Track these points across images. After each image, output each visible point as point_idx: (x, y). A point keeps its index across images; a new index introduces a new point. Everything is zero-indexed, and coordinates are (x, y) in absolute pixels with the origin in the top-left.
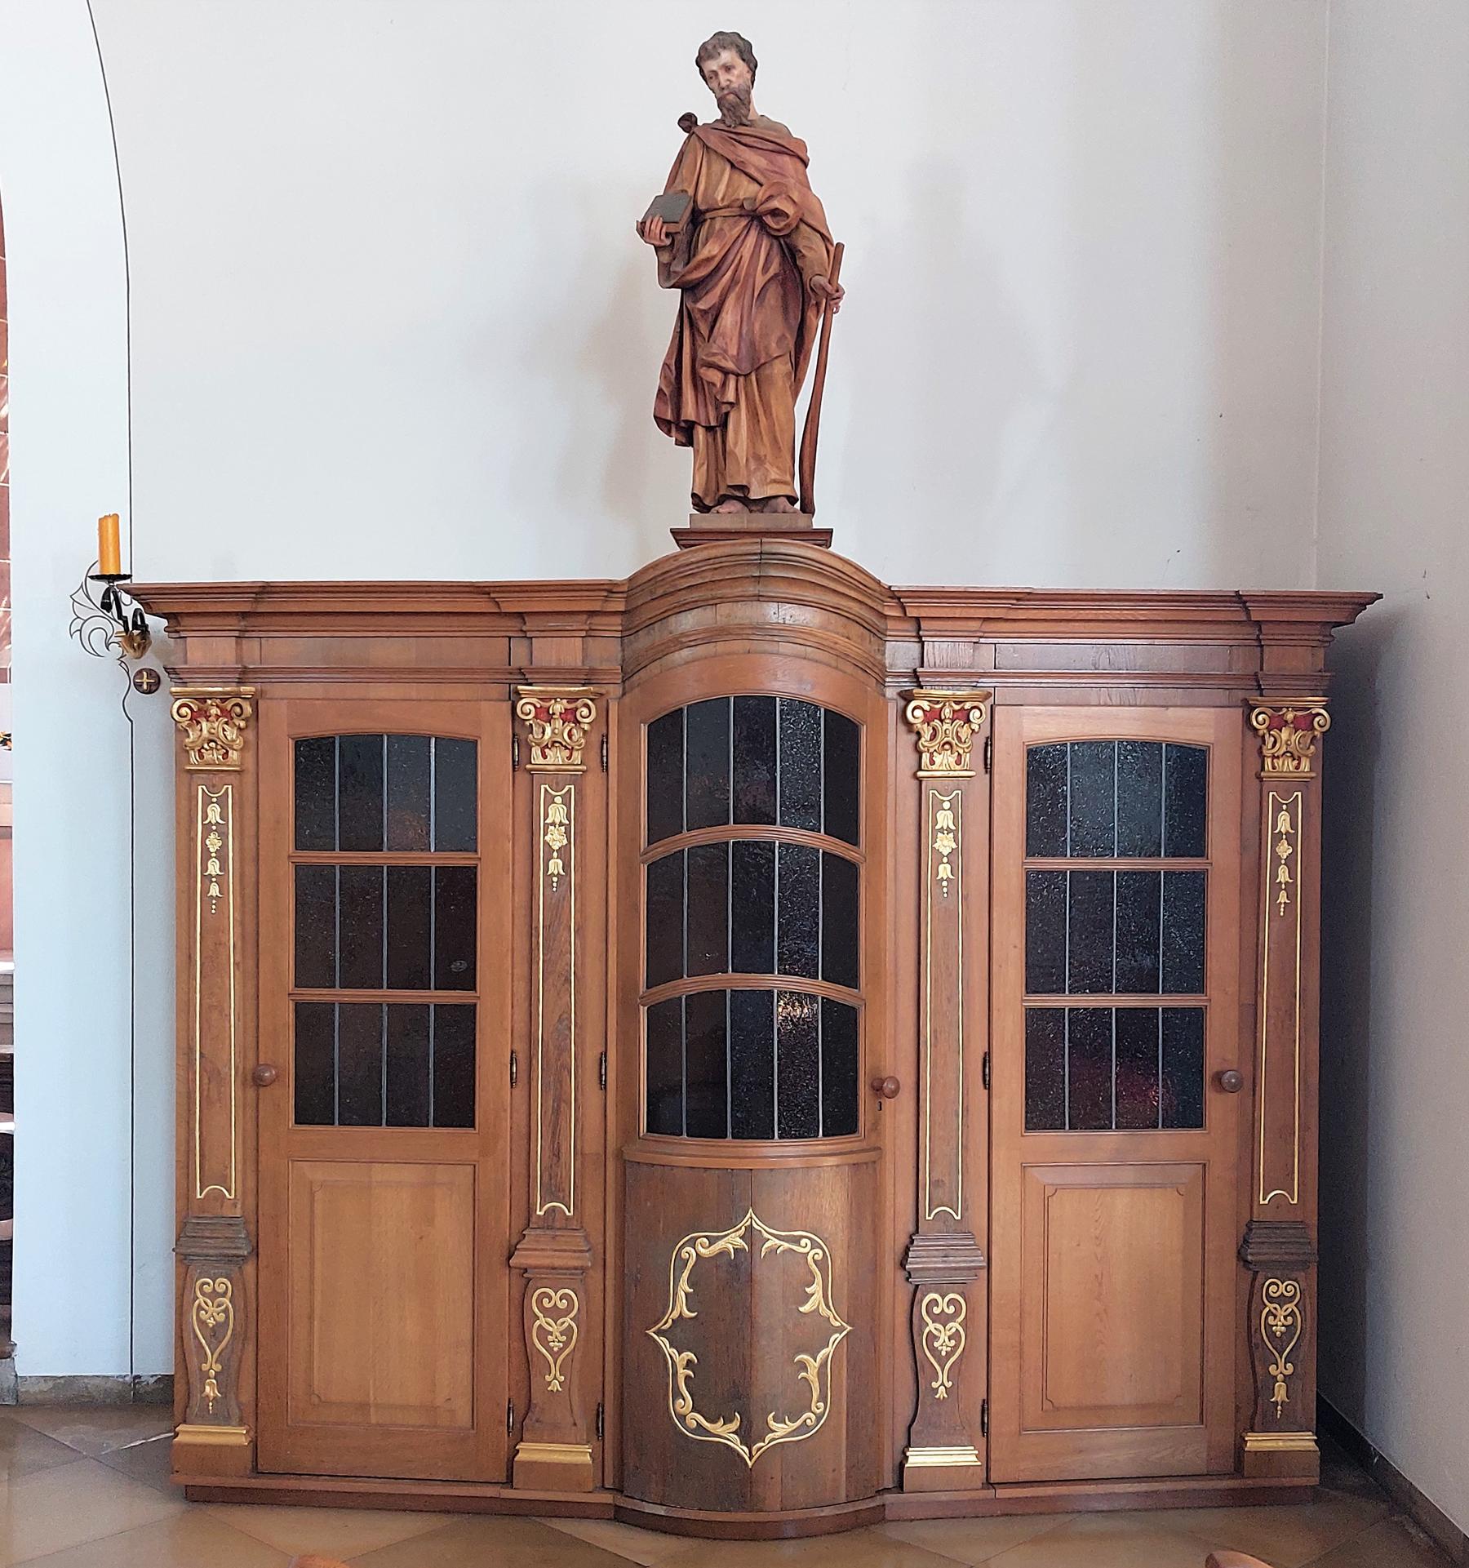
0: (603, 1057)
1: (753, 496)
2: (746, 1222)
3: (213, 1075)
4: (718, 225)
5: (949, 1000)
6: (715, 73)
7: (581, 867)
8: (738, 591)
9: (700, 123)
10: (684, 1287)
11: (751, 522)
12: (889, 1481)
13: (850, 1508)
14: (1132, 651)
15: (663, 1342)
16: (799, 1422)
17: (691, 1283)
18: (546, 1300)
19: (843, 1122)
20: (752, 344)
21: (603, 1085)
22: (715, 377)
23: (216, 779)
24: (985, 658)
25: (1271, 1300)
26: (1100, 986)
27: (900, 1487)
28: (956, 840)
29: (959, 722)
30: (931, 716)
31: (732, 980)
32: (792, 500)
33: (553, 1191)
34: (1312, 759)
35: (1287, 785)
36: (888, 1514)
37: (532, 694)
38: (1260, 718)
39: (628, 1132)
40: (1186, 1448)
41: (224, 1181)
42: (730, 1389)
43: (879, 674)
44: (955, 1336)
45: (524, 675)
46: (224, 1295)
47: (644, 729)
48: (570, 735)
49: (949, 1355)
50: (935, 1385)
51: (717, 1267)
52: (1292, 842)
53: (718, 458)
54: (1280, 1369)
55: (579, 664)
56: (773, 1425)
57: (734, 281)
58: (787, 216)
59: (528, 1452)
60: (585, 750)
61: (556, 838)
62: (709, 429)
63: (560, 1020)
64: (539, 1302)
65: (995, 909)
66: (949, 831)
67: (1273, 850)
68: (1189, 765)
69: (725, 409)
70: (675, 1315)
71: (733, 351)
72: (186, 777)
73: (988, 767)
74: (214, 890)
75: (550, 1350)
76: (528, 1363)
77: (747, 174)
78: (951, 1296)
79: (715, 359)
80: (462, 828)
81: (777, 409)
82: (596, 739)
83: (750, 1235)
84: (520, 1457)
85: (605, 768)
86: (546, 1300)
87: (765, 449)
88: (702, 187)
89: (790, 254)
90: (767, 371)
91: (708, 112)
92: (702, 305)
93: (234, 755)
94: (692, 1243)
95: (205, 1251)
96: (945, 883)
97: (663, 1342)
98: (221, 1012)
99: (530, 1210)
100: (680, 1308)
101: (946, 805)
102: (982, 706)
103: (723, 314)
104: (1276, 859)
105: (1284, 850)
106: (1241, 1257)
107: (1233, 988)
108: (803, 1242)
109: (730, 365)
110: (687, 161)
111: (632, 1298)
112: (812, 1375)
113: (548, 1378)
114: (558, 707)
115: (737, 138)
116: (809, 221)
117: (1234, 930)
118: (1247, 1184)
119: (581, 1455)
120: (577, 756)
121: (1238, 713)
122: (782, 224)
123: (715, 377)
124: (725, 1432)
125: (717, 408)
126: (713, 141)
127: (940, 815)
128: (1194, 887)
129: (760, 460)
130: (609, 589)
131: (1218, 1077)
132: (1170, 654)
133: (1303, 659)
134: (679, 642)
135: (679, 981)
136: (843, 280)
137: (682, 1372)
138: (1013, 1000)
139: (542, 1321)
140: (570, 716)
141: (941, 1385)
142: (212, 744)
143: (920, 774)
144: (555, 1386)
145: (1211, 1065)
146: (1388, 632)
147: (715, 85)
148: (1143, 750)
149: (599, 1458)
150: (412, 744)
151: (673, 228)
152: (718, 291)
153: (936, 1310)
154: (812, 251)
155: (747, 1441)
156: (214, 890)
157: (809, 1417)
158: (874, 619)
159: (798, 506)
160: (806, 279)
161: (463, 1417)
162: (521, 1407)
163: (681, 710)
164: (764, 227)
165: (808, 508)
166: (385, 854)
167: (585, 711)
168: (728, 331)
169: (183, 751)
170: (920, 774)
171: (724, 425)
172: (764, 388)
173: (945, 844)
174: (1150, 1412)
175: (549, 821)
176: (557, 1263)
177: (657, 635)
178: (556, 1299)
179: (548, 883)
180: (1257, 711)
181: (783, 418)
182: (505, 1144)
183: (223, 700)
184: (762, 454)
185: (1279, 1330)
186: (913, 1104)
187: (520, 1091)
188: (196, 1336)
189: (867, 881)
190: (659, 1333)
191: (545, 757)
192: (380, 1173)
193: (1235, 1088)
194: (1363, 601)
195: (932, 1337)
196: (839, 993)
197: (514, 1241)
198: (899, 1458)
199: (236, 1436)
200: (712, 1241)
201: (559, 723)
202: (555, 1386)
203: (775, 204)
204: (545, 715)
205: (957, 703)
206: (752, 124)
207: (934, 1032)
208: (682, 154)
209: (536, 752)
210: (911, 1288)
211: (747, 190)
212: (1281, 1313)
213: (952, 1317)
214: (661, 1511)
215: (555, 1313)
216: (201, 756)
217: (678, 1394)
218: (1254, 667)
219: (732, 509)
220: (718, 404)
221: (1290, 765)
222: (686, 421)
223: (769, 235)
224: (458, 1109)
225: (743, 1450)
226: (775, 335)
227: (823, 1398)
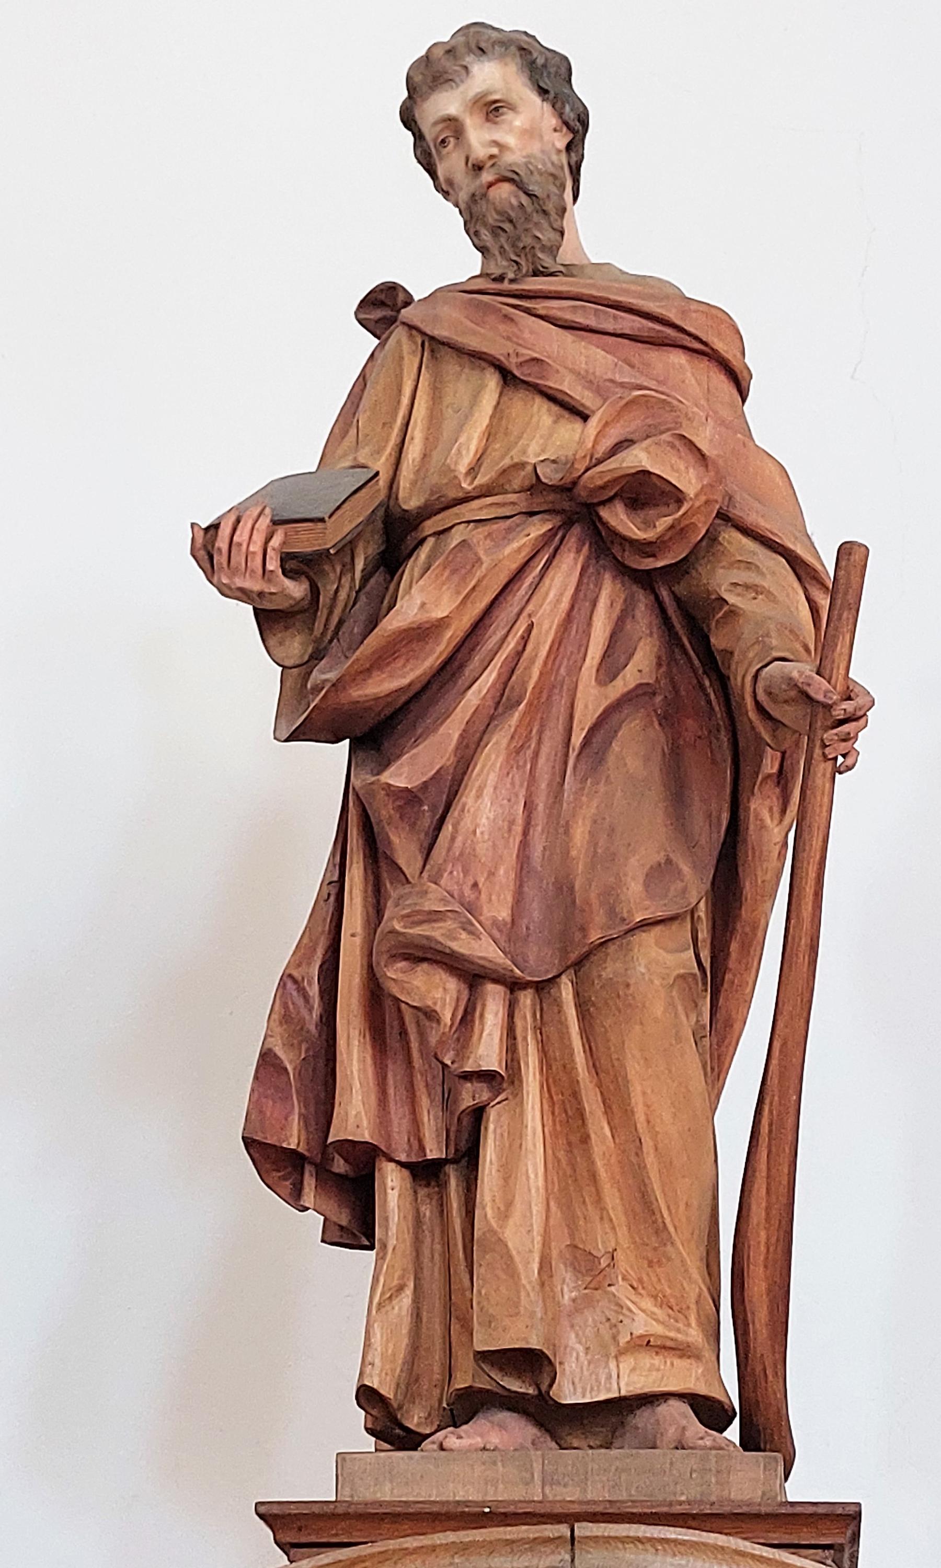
1: (569, 1392)
6: (454, 126)
20: (564, 888)
22: (439, 991)
32: (712, 1413)
57: (502, 700)
58: (676, 496)
62: (424, 1173)
69: (469, 1095)
77: (552, 397)
79: (436, 932)
81: (645, 1089)
87: (612, 1234)
88: (413, 451)
89: (692, 628)
90: (609, 968)
91: (437, 254)
103: (468, 798)
109: (484, 950)
116: (749, 516)
122: (663, 523)
123: (439, 991)
125: (448, 1101)
126: (451, 324)
129: (592, 1269)
136: (871, 660)
152: (451, 730)
154: (762, 608)
159: (733, 1432)
160: (741, 676)
164: (605, 547)
165: (764, 1429)
168: (483, 849)
171: (468, 1156)
172: (605, 1021)
184: (600, 1249)
203: (640, 458)
206: (569, 270)
208: (363, 377)
211: (548, 441)
219: (494, 1439)
222: (349, 1148)
223: (624, 572)
226: (632, 839)
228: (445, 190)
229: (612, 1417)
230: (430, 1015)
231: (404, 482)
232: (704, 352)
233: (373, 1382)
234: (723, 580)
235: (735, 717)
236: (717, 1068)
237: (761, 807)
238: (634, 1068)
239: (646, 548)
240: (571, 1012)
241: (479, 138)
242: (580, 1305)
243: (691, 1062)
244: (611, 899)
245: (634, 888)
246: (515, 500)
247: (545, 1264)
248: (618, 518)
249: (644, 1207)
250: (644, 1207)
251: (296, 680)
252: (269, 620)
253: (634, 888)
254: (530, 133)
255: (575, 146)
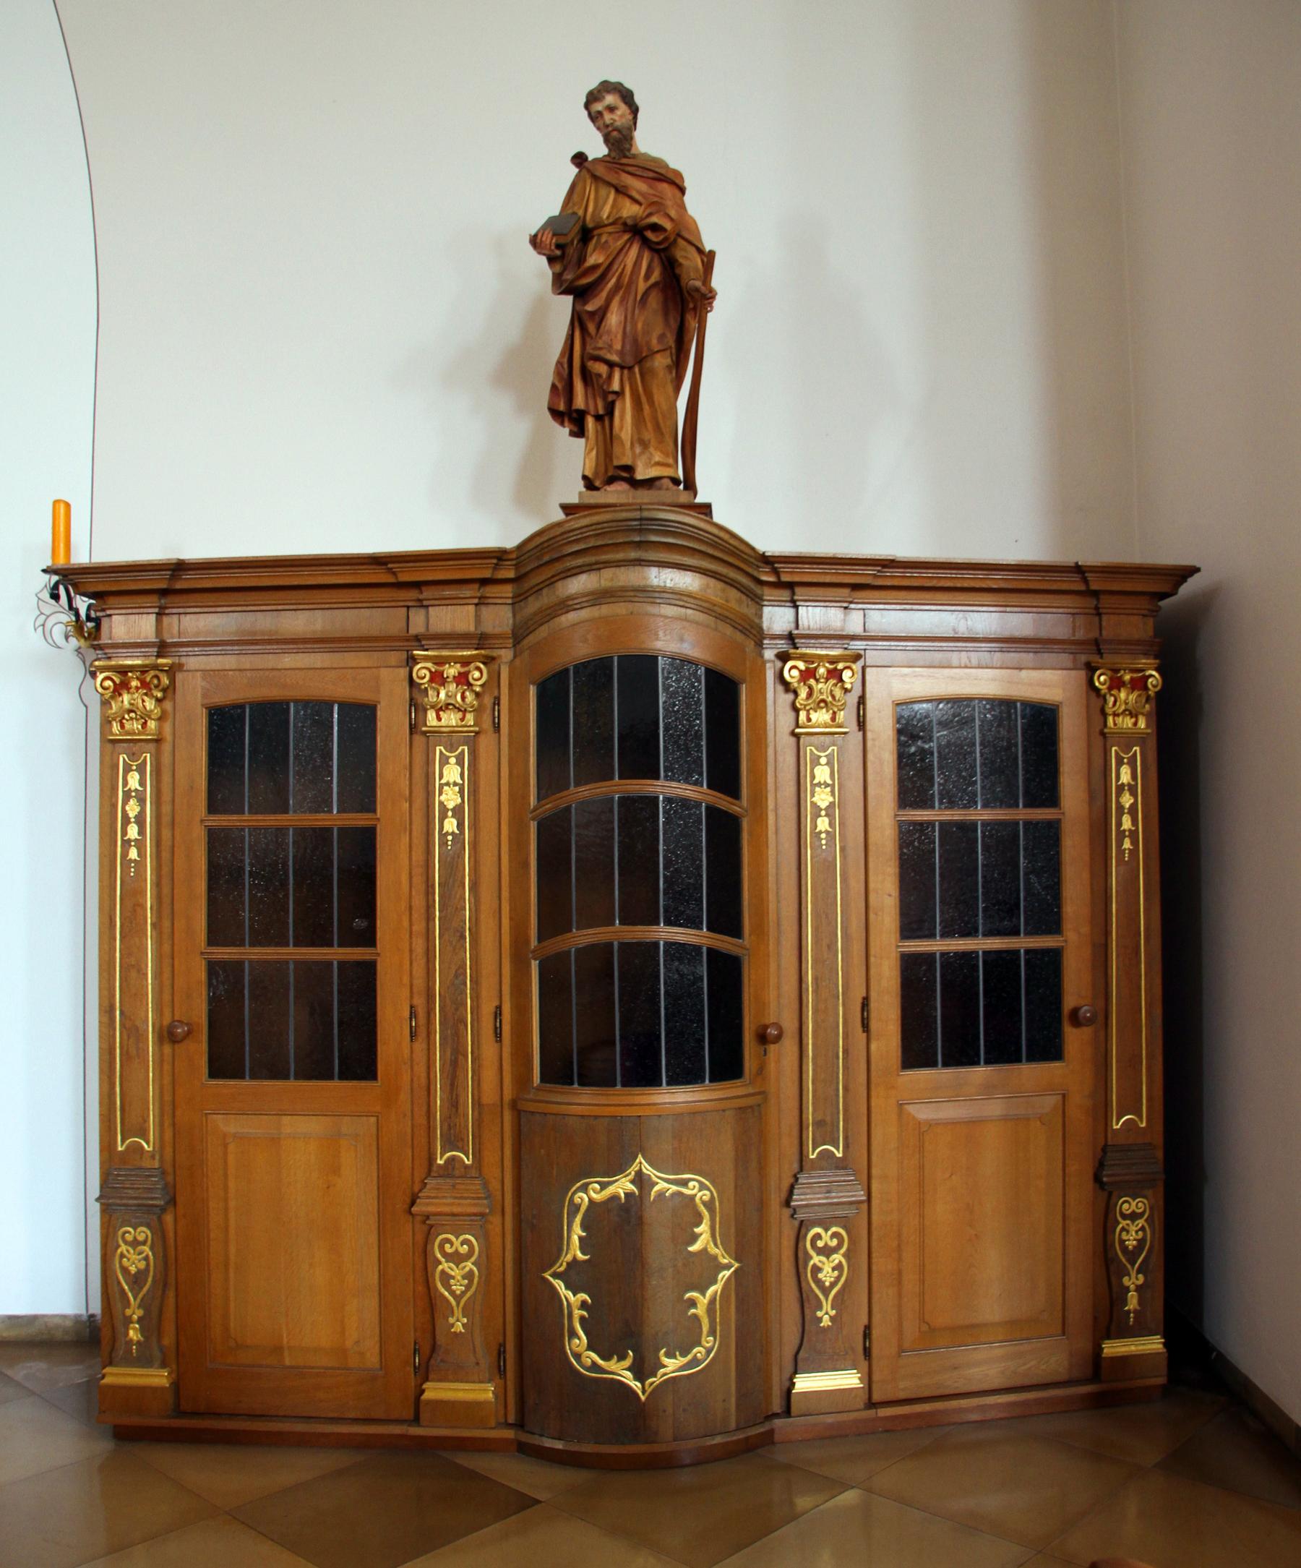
0: (498, 1012)
1: (641, 474)
2: (635, 1167)
3: (133, 1031)
4: (603, 239)
5: (829, 947)
6: (600, 113)
7: (475, 826)
8: (620, 556)
9: (590, 159)
10: (578, 1231)
11: (638, 497)
12: (777, 1406)
13: (740, 1436)
14: (984, 620)
15: (559, 1285)
16: (690, 1357)
17: (584, 1226)
18: (447, 1246)
19: (728, 1066)
20: (635, 341)
21: (498, 1034)
22: (602, 369)
23: (136, 748)
24: (854, 621)
25: (1124, 1217)
26: (970, 932)
27: (787, 1412)
28: (833, 793)
29: (832, 682)
30: (807, 675)
31: (619, 933)
32: (676, 481)
33: (453, 1141)
34: (1147, 716)
35: (1127, 740)
36: (777, 1437)
37: (426, 659)
38: (1102, 678)
39: (522, 1080)
40: (1050, 1358)
41: (143, 1134)
42: (621, 1328)
43: (758, 635)
44: (838, 1267)
45: (418, 640)
46: (144, 1243)
47: (532, 690)
48: (463, 698)
49: (833, 1285)
50: (819, 1314)
51: (609, 1211)
52: (1133, 792)
53: (608, 442)
54: (1133, 1280)
55: (472, 629)
56: (665, 1360)
57: (618, 287)
59: (434, 1391)
60: (478, 711)
61: (451, 798)
62: (598, 418)
63: (456, 976)
64: (441, 1247)
65: (871, 859)
66: (827, 785)
67: (1118, 802)
68: (1041, 720)
69: (611, 398)
70: (569, 1258)
71: (618, 346)
72: (109, 746)
73: (862, 725)
74: (133, 854)
75: (452, 1293)
76: (432, 1306)
78: (834, 1229)
79: (602, 353)
80: (362, 791)
81: (659, 397)
82: (488, 701)
83: (640, 1179)
84: (427, 1395)
85: (497, 728)
86: (447, 1246)
87: (649, 435)
89: (670, 266)
90: (648, 364)
91: (596, 148)
92: (590, 308)
93: (152, 725)
94: (584, 1188)
95: (124, 1201)
96: (823, 836)
97: (559, 1285)
98: (139, 971)
99: (431, 1159)
100: (575, 1251)
101: (823, 760)
102: (854, 667)
104: (1120, 808)
105: (1127, 800)
106: (1097, 1179)
107: (1085, 929)
108: (691, 1184)
109: (614, 358)
110: (578, 189)
111: (532, 1241)
112: (700, 1310)
113: (451, 1320)
114: (451, 671)
115: (623, 168)
116: (685, 233)
117: (1086, 875)
118: (1101, 1112)
119: (485, 1392)
120: (470, 718)
121: (1082, 674)
123: (602, 369)
124: (621, 1371)
125: (605, 398)
126: (600, 171)
127: (817, 770)
128: (1048, 837)
129: (645, 445)
130: (499, 556)
131: (1075, 1013)
132: (1018, 622)
133: (1137, 627)
134: (565, 605)
135: (568, 935)
136: (716, 282)
137: (577, 1313)
138: (889, 947)
139: (445, 1265)
140: (462, 679)
141: (826, 1315)
142: (133, 715)
143: (798, 730)
144: (459, 1327)
145: (1069, 1002)
146: (1203, 608)
147: (600, 123)
148: (1004, 706)
149: (501, 1395)
150: (317, 709)
151: (562, 241)
152: (604, 294)
153: (820, 1244)
154: (689, 262)
155: (640, 1374)
156: (133, 854)
157: (698, 1351)
158: (752, 585)
159: (681, 487)
160: (683, 283)
161: (373, 1359)
162: (426, 1349)
163: (567, 670)
164: (646, 242)
165: (690, 485)
166: (290, 816)
167: (477, 674)
168: (614, 329)
169: (106, 722)
170: (798, 730)
173: (823, 798)
174: (1016, 1329)
175: (443, 781)
176: (456, 1210)
177: (546, 598)
178: (458, 1244)
179: (443, 843)
180: (1098, 673)
181: (665, 407)
182: (404, 1096)
183: (143, 672)
185: (1131, 1244)
186: (795, 1049)
187: (420, 1046)
188: (119, 1283)
189: (751, 834)
190: (555, 1275)
191: (439, 719)
192: (290, 1125)
193: (1090, 1022)
194: (1188, 572)
195: (816, 1270)
196: (724, 943)
197: (416, 1190)
198: (787, 1384)
199: (159, 1378)
200: (604, 1186)
201: (452, 687)
202: (459, 1327)
203: (654, 219)
204: (438, 678)
205: (831, 663)
206: (634, 157)
207: (815, 979)
209: (431, 715)
210: (796, 1223)
211: (629, 210)
212: (1133, 1229)
213: (835, 1250)
214: (559, 1445)
215: (457, 1258)
216: (122, 726)
217: (573, 1334)
218: (1094, 634)
220: (605, 397)
221: (1129, 722)
224: (359, 1062)
225: (636, 1385)
226: (655, 328)
227: (712, 1332)
228: (598, 129)
229: (650, 483)
230: (600, 375)
231: (588, 218)
232: (672, 183)
233: (587, 473)
234: (679, 255)
235: (682, 294)
236: (677, 389)
237: (689, 317)
238: (655, 391)
239: (658, 243)
240: (638, 376)
241: (608, 117)
242: (642, 453)
243: (670, 388)
244: (648, 343)
245: (654, 342)
246: (619, 227)
247: (632, 444)
248: (649, 234)
249: (657, 427)
250: (657, 427)
251: (557, 279)
252: (551, 260)
253: (654, 342)
254: (621, 116)
255: (635, 118)
